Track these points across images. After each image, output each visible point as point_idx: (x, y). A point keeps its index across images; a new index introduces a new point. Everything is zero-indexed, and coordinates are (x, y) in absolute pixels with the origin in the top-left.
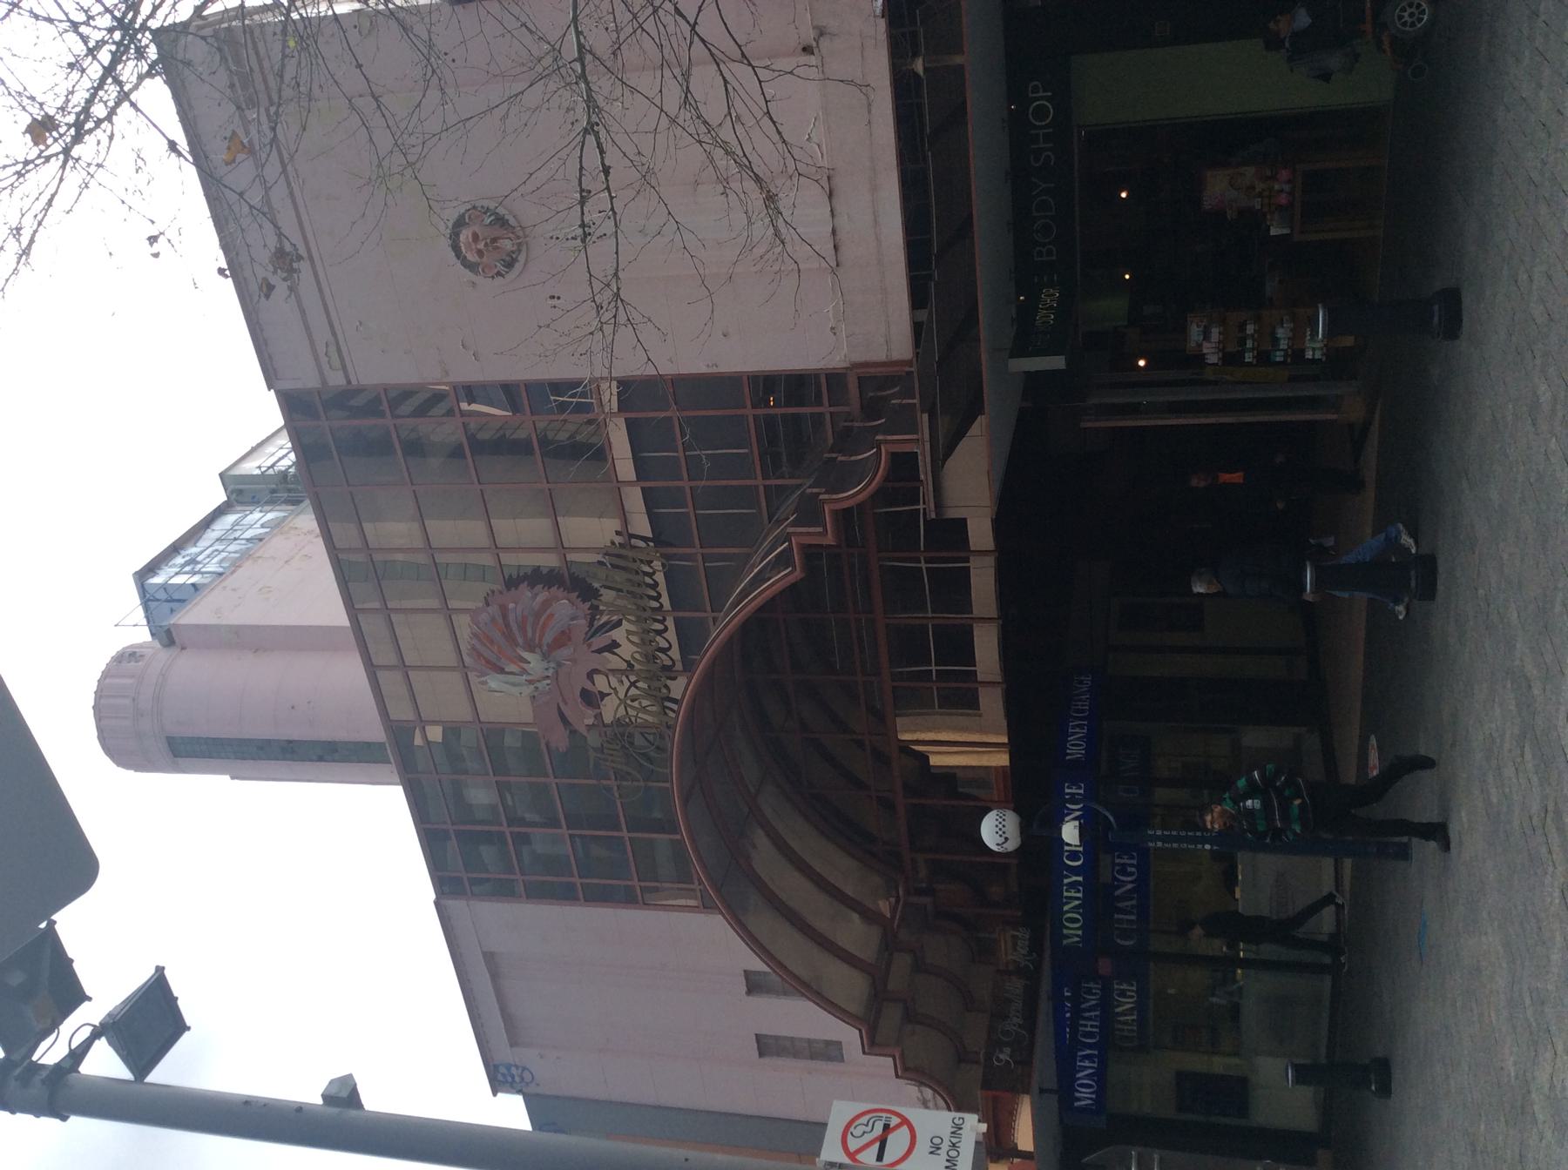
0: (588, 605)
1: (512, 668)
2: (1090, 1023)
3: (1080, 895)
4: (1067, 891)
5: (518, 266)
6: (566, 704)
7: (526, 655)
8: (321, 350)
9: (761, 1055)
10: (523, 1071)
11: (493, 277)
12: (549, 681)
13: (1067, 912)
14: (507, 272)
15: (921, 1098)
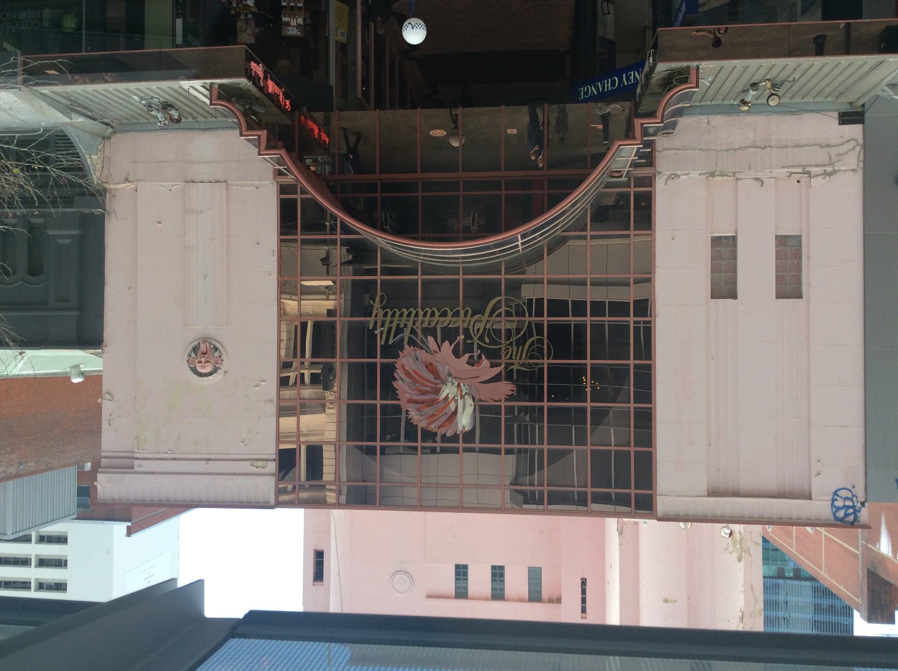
0: (406, 346)
1: (452, 406)
5: (218, 345)
6: (478, 377)
7: (443, 396)
9: (799, 296)
10: (837, 495)
11: (222, 360)
12: (462, 385)
14: (220, 351)
15: (823, 176)
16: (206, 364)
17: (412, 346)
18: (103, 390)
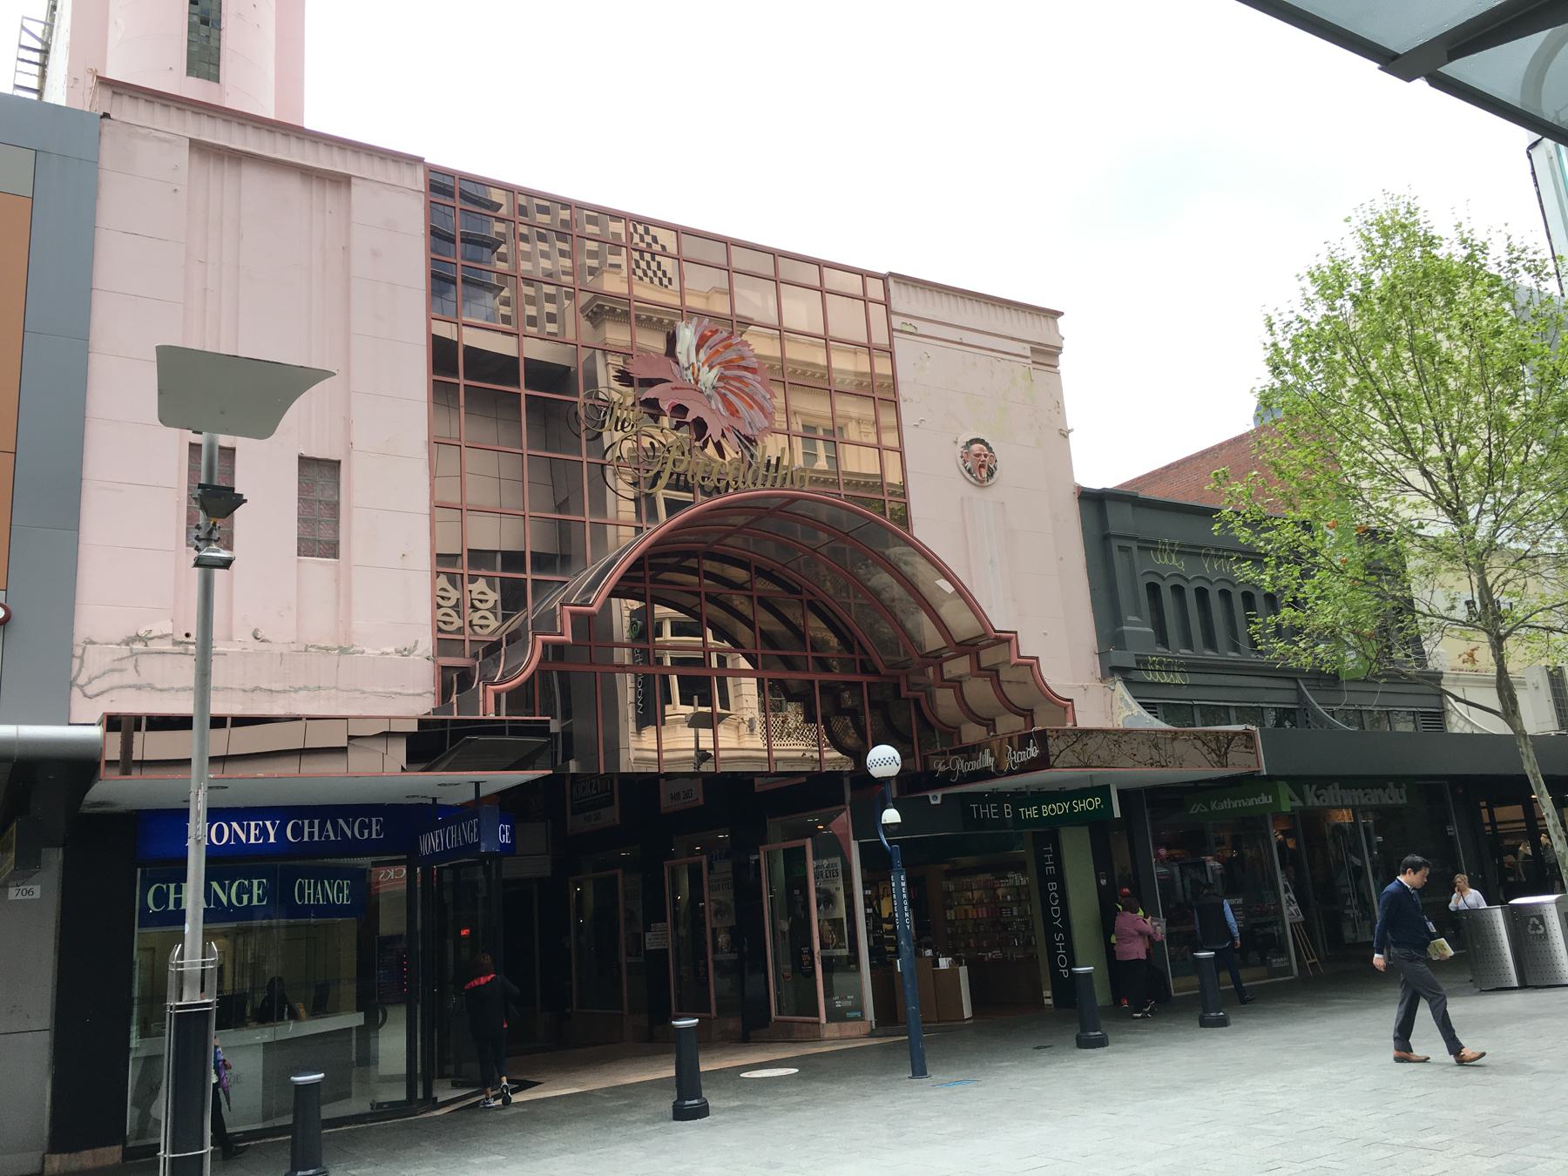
2: (316, 830)
3: (252, 841)
4: (257, 825)
6: (673, 389)
7: (715, 371)
8: (915, 322)
13: (230, 827)
16: (978, 452)
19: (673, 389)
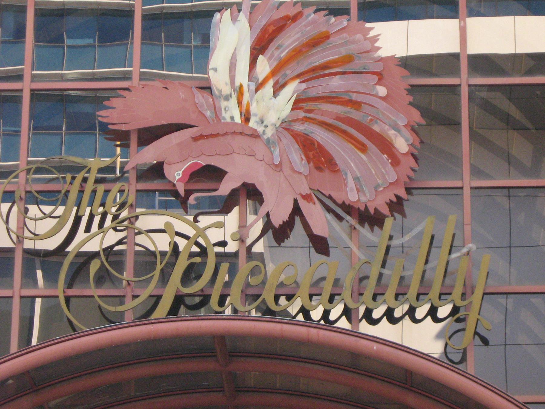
6: (195, 139)
17: (372, 211)
18: (154, 301)
19: (195, 139)
